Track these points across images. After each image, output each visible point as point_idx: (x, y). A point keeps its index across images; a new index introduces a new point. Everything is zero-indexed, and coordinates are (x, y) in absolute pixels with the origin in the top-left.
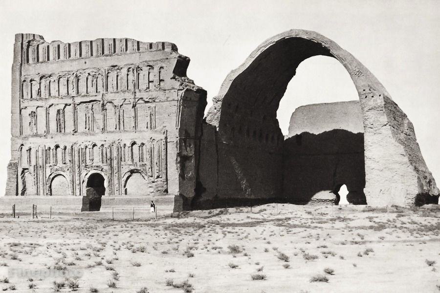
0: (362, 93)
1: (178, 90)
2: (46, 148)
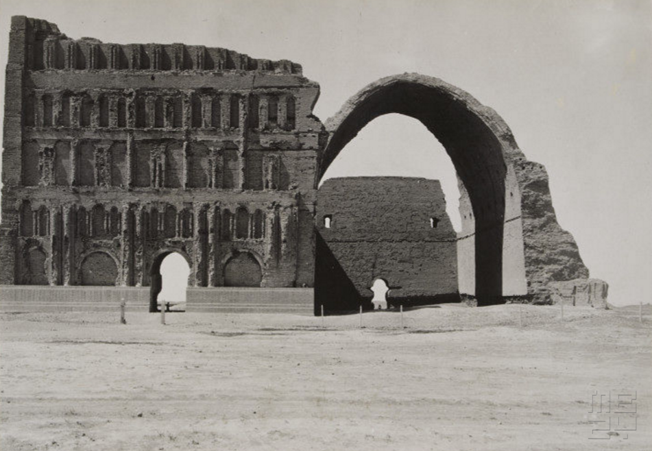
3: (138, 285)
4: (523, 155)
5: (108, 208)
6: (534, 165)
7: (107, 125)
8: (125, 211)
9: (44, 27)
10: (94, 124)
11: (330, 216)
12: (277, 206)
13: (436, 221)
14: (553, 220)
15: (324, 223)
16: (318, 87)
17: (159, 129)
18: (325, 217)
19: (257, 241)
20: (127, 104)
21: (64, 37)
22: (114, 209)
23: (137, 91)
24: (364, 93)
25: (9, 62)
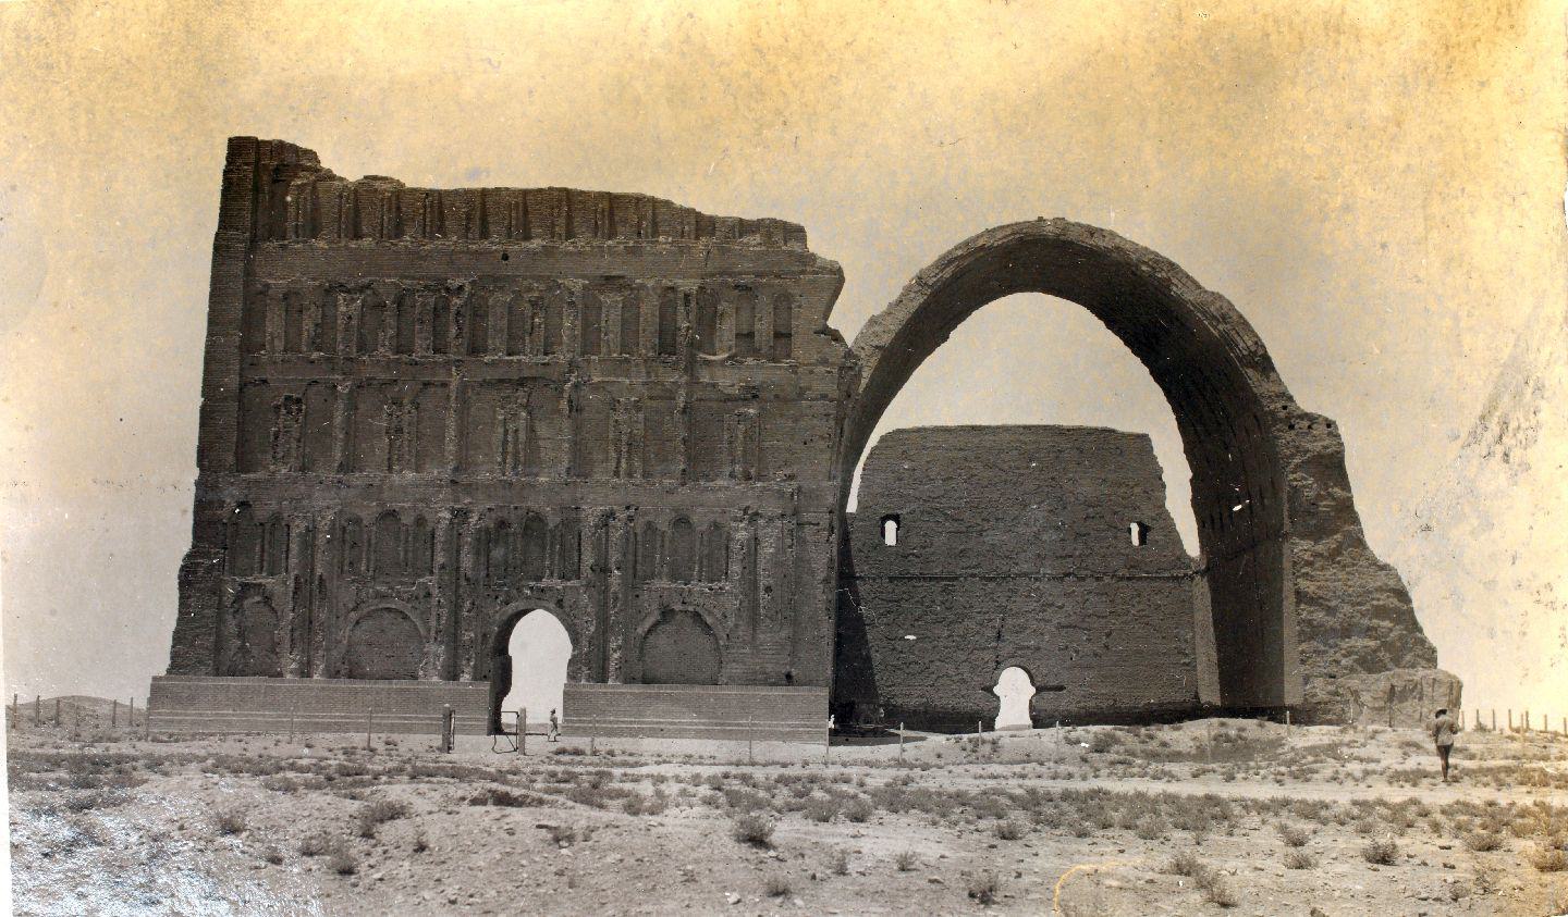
4: (1290, 398)
5: (407, 520)
6: (1311, 419)
7: (410, 352)
8: (444, 524)
9: (290, 158)
10: (384, 352)
11: (896, 518)
13: (1144, 531)
14: (1359, 542)
15: (883, 534)
16: (840, 271)
17: (515, 358)
18: (885, 519)
19: (711, 589)
20: (453, 310)
21: (330, 176)
22: (420, 521)
23: (473, 283)
24: (950, 262)
25: (219, 228)
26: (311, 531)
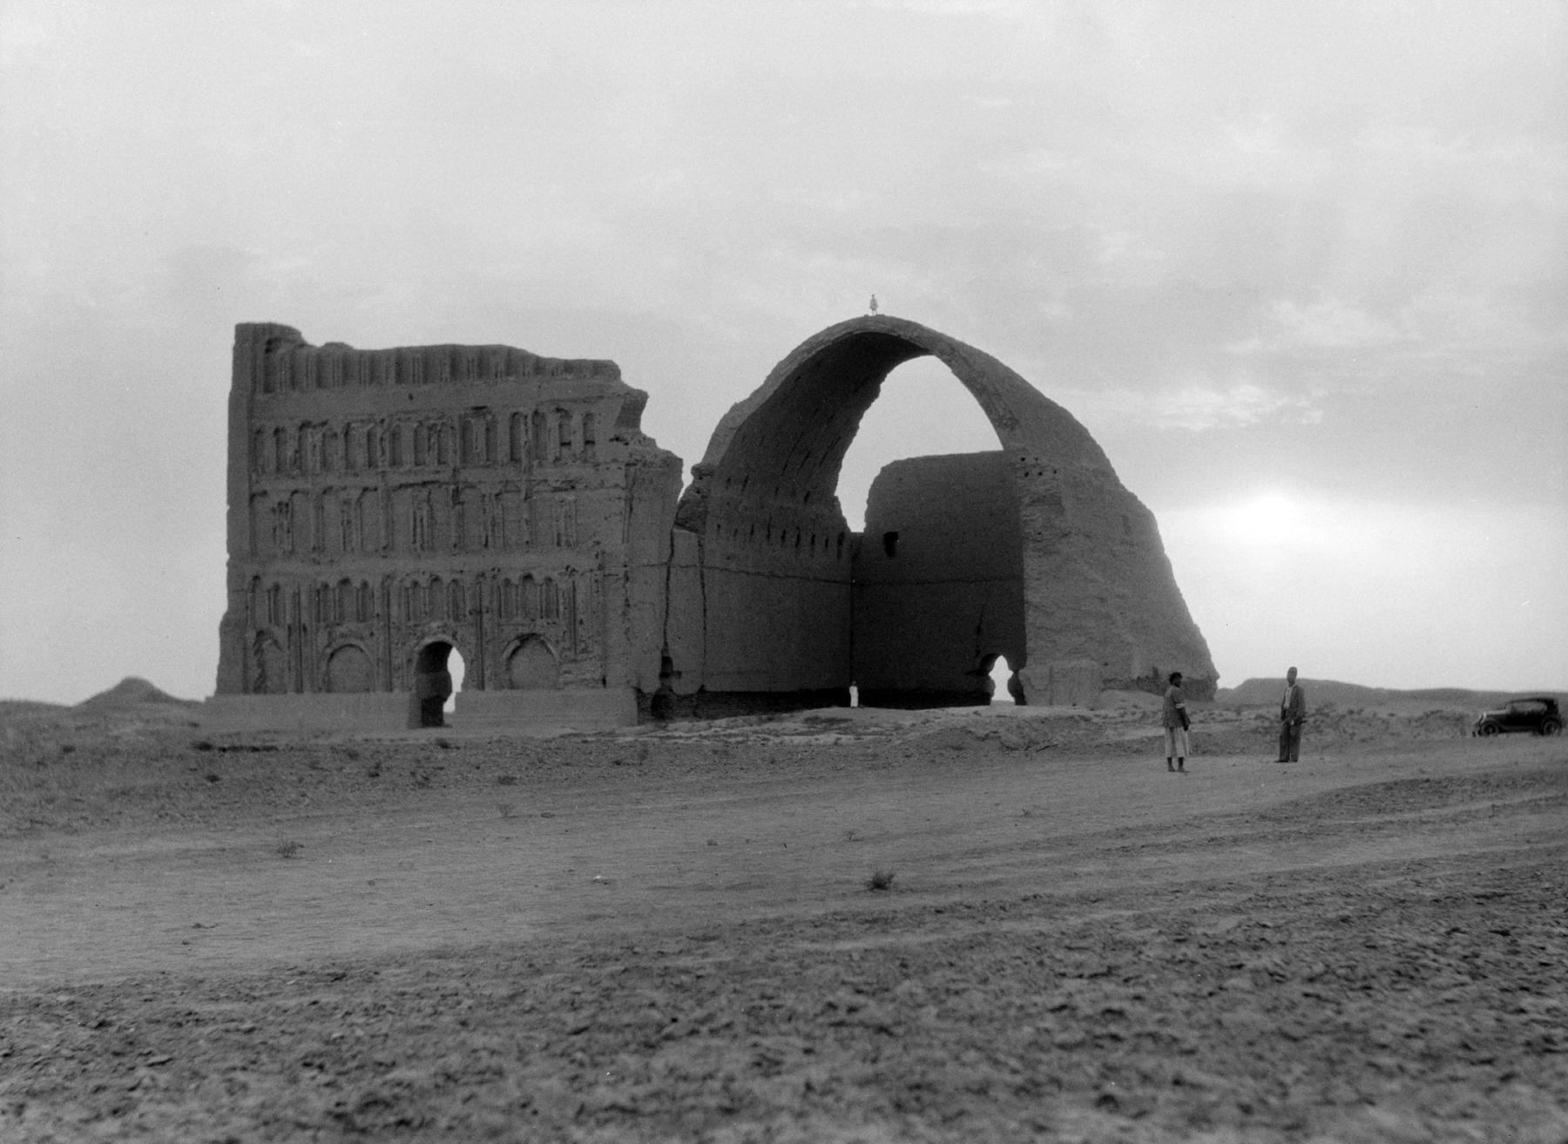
0: (1018, 466)
1: (627, 465)
2: (319, 586)
3: (396, 691)
12: (570, 571)
26: (297, 595)
